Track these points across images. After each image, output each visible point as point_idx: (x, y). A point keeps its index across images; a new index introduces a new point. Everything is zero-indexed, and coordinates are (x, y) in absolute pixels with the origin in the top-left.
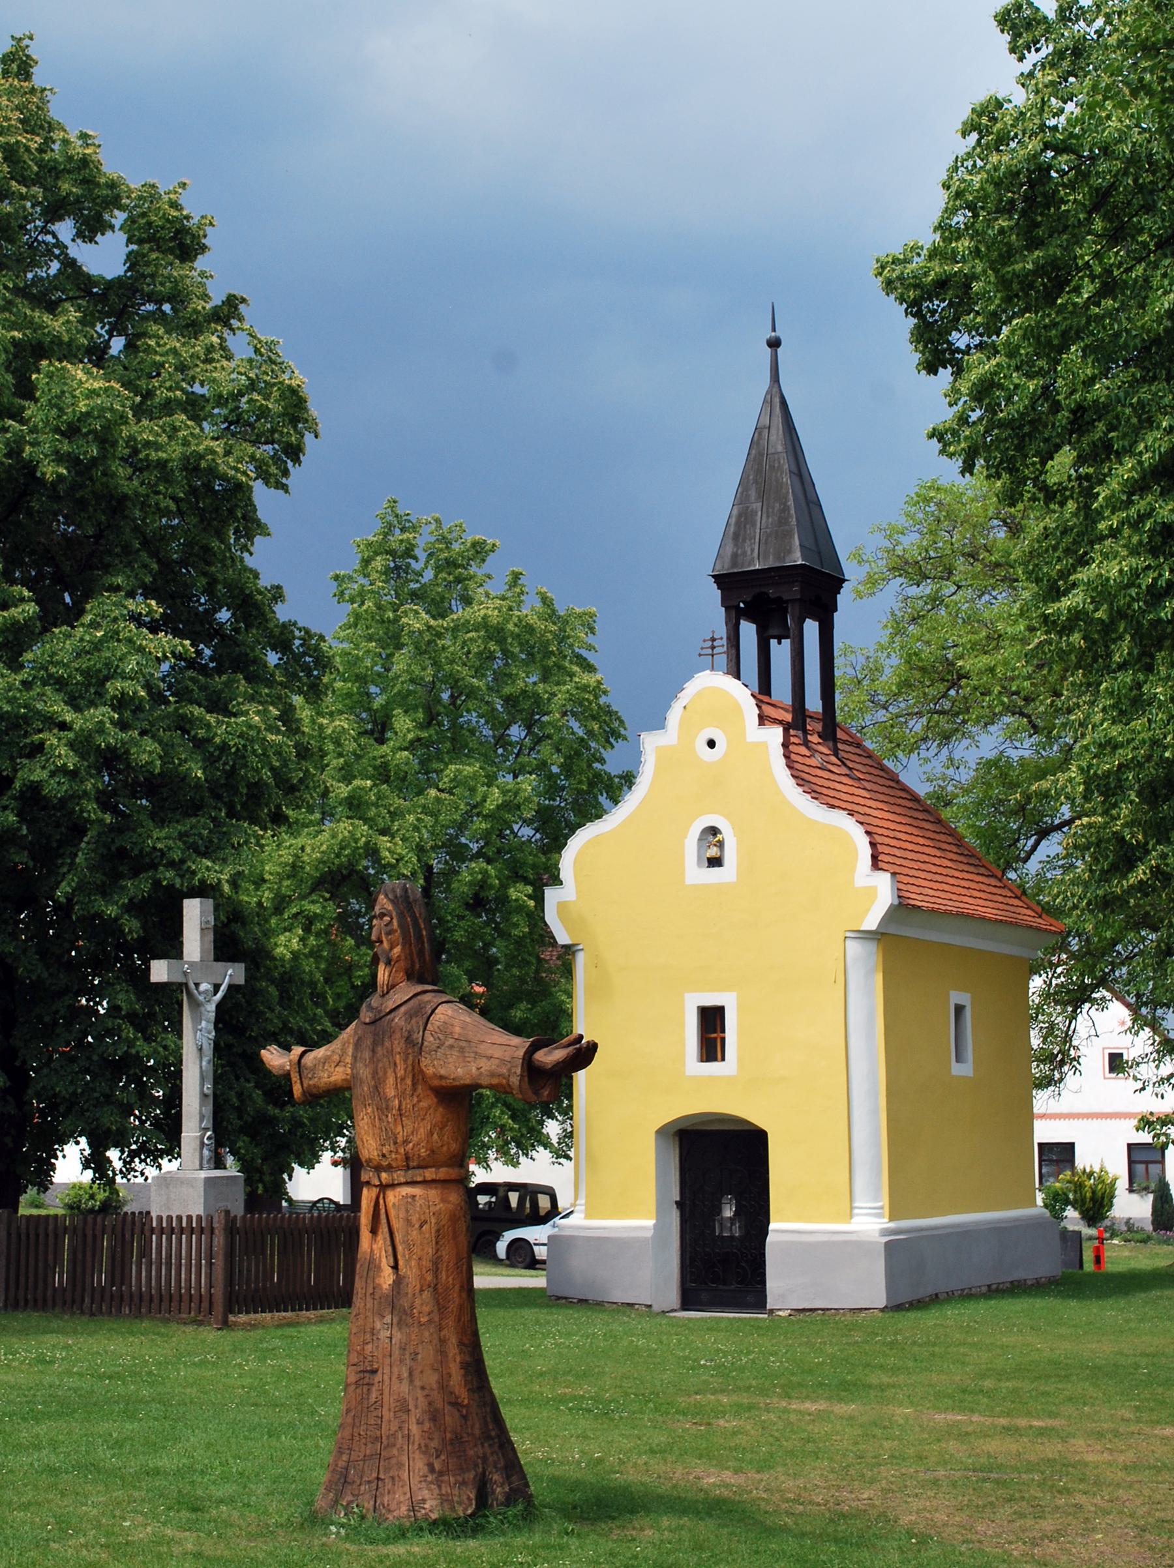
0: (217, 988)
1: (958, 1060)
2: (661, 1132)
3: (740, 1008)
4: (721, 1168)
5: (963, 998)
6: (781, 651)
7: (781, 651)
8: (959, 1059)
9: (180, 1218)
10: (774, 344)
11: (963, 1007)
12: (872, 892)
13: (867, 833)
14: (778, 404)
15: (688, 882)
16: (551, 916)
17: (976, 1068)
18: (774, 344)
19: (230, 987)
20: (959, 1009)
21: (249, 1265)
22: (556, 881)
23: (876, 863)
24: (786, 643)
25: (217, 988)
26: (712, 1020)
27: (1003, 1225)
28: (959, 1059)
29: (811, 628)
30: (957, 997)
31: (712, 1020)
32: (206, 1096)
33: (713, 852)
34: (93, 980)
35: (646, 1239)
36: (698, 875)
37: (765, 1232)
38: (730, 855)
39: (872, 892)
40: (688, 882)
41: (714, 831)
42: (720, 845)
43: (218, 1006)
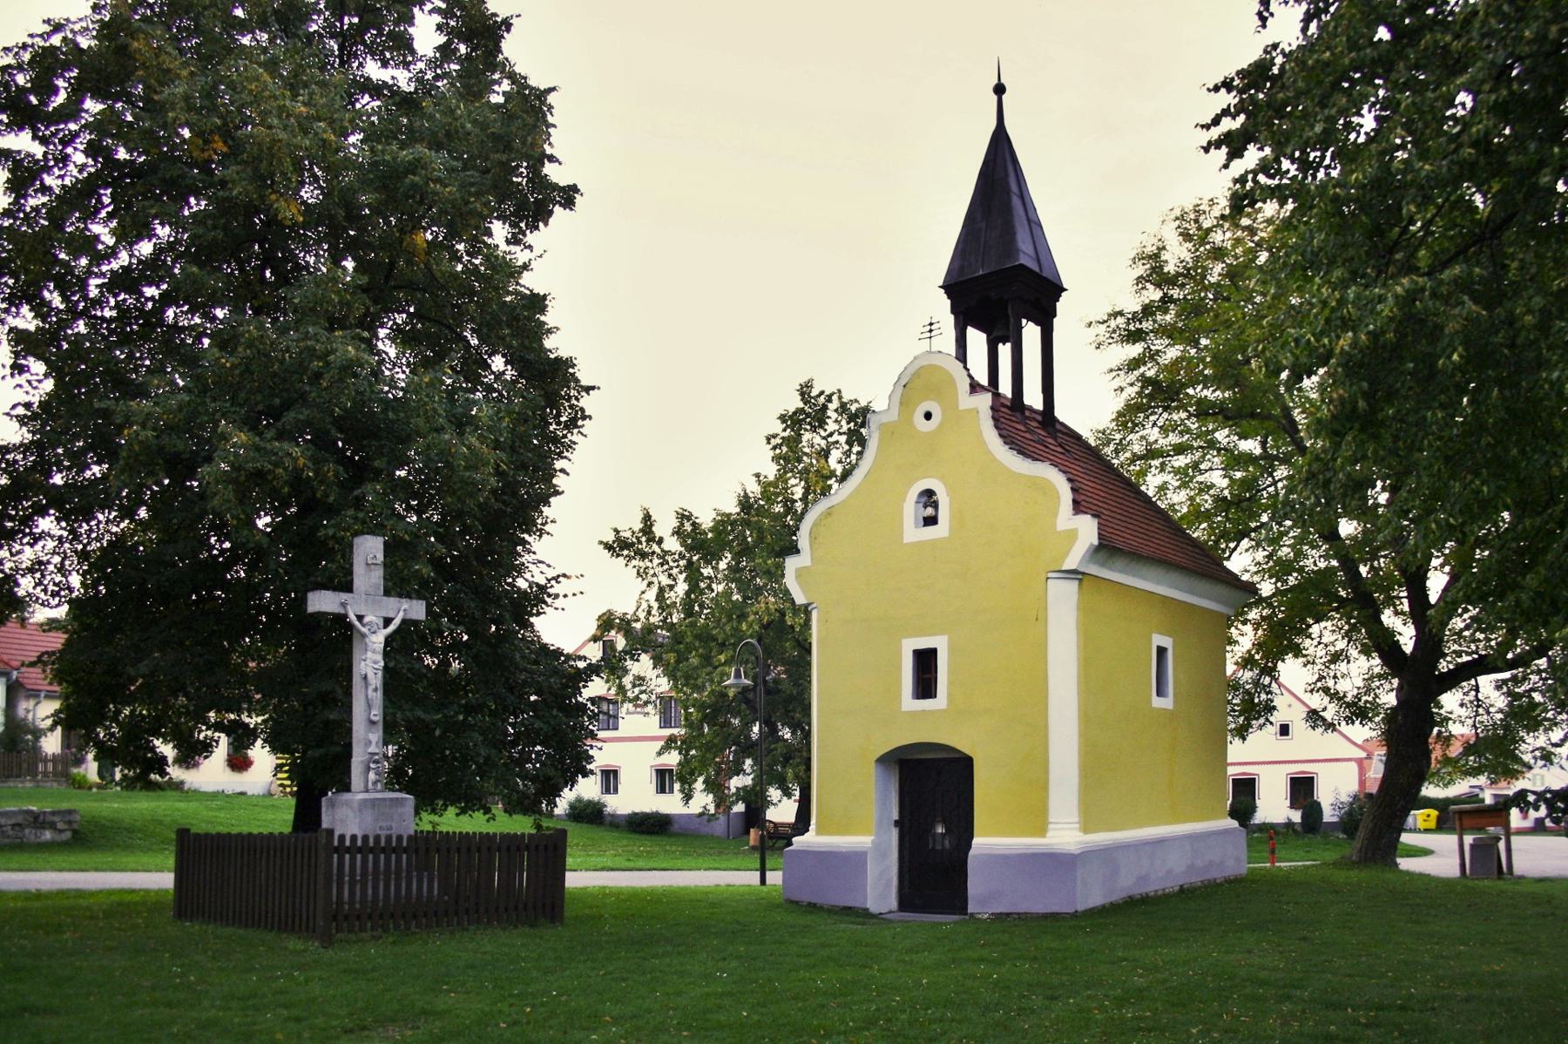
0: (387, 622)
1: (1159, 694)
2: (884, 760)
3: (952, 650)
4: (932, 788)
5: (1166, 642)
6: (1005, 351)
7: (1005, 351)
8: (1160, 692)
9: (342, 837)
10: (1000, 90)
11: (932, 653)
12: (1072, 535)
13: (1069, 480)
14: (1000, 146)
15: (906, 541)
16: (790, 581)
17: (1175, 702)
18: (1000, 90)
19: (404, 621)
20: (1161, 651)
21: (420, 888)
22: (794, 550)
23: (1078, 507)
24: (1008, 345)
25: (387, 622)
26: (925, 661)
27: (127, 898)
28: (1160, 692)
29: (1031, 333)
30: (1159, 640)
31: (925, 661)
32: (373, 723)
33: (930, 511)
34: (747, 726)
35: (160, 892)
36: (914, 533)
37: (969, 846)
38: (910, 509)
39: (1072, 535)
40: (906, 541)
41: (929, 494)
42: (935, 505)
43: (389, 641)
